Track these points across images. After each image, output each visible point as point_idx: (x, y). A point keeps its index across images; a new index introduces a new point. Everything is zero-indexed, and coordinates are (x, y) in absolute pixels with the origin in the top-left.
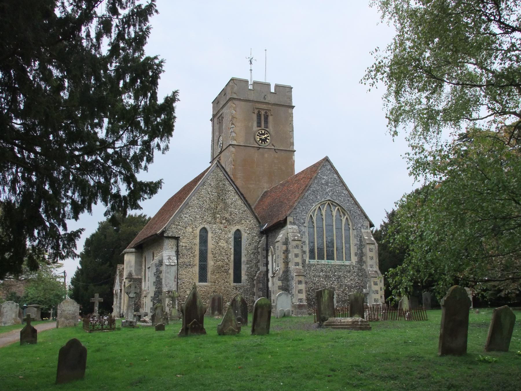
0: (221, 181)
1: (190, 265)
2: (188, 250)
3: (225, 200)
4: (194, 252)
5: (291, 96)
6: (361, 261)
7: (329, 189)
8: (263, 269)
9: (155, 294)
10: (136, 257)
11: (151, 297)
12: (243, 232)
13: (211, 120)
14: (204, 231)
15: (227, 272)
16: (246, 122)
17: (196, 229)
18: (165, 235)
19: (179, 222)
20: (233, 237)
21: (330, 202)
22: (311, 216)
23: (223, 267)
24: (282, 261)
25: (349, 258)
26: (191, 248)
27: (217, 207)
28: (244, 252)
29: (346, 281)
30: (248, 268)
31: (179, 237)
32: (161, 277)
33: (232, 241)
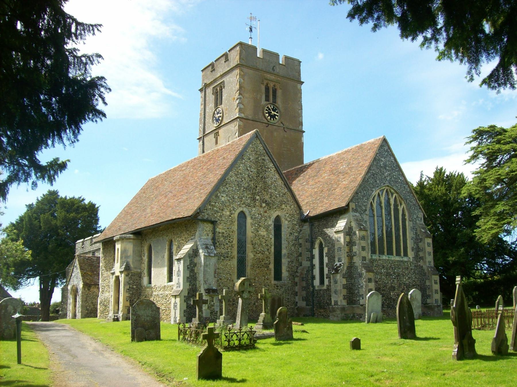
0: (260, 155)
1: (227, 257)
2: (225, 237)
3: (265, 178)
4: (232, 242)
5: (300, 70)
6: (417, 258)
7: (387, 174)
8: (306, 264)
9: (189, 293)
10: (134, 245)
11: (185, 296)
12: (283, 219)
13: (201, 90)
14: (242, 215)
15: (267, 266)
16: (255, 94)
17: (234, 212)
18: (199, 217)
19: (215, 203)
20: (273, 225)
21: (388, 188)
22: (371, 202)
23: (263, 260)
24: (346, 255)
25: (406, 254)
26: (229, 236)
27: (256, 187)
28: (284, 244)
29: (405, 280)
30: (289, 262)
31: (216, 222)
32: (196, 271)
33: (272, 228)
